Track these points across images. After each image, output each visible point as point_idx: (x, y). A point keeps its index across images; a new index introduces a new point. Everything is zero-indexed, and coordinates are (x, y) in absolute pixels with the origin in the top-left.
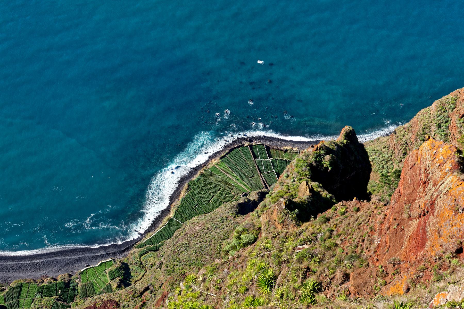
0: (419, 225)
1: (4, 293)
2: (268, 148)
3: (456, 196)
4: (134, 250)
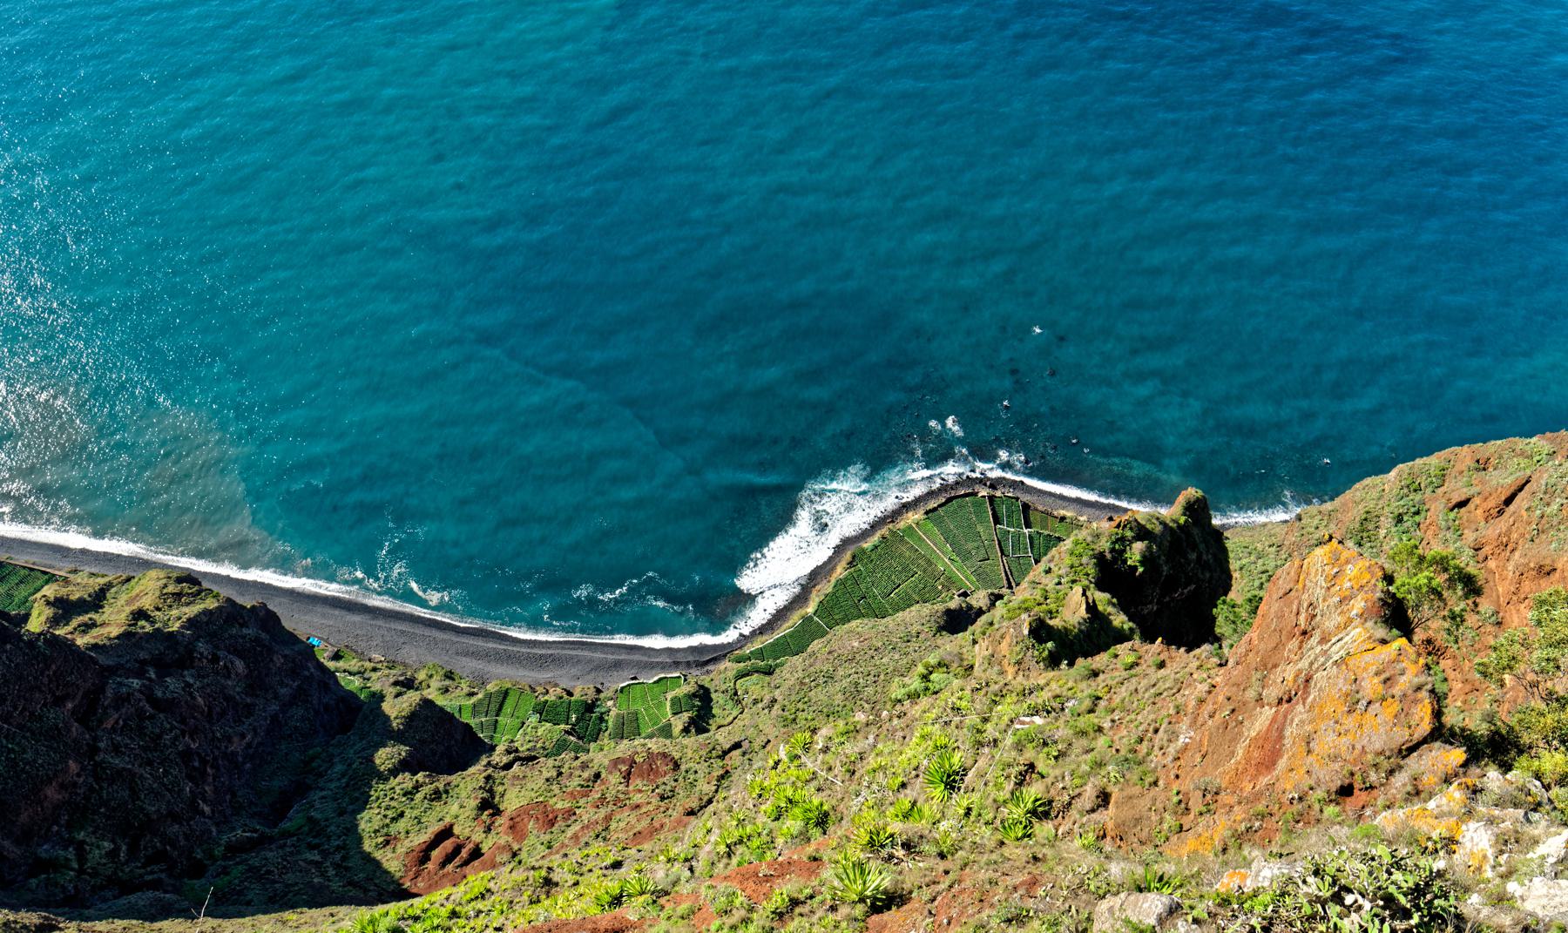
0: (1274, 720)
1: (474, 699)
2: (1026, 507)
3: (1359, 672)
4: (725, 664)
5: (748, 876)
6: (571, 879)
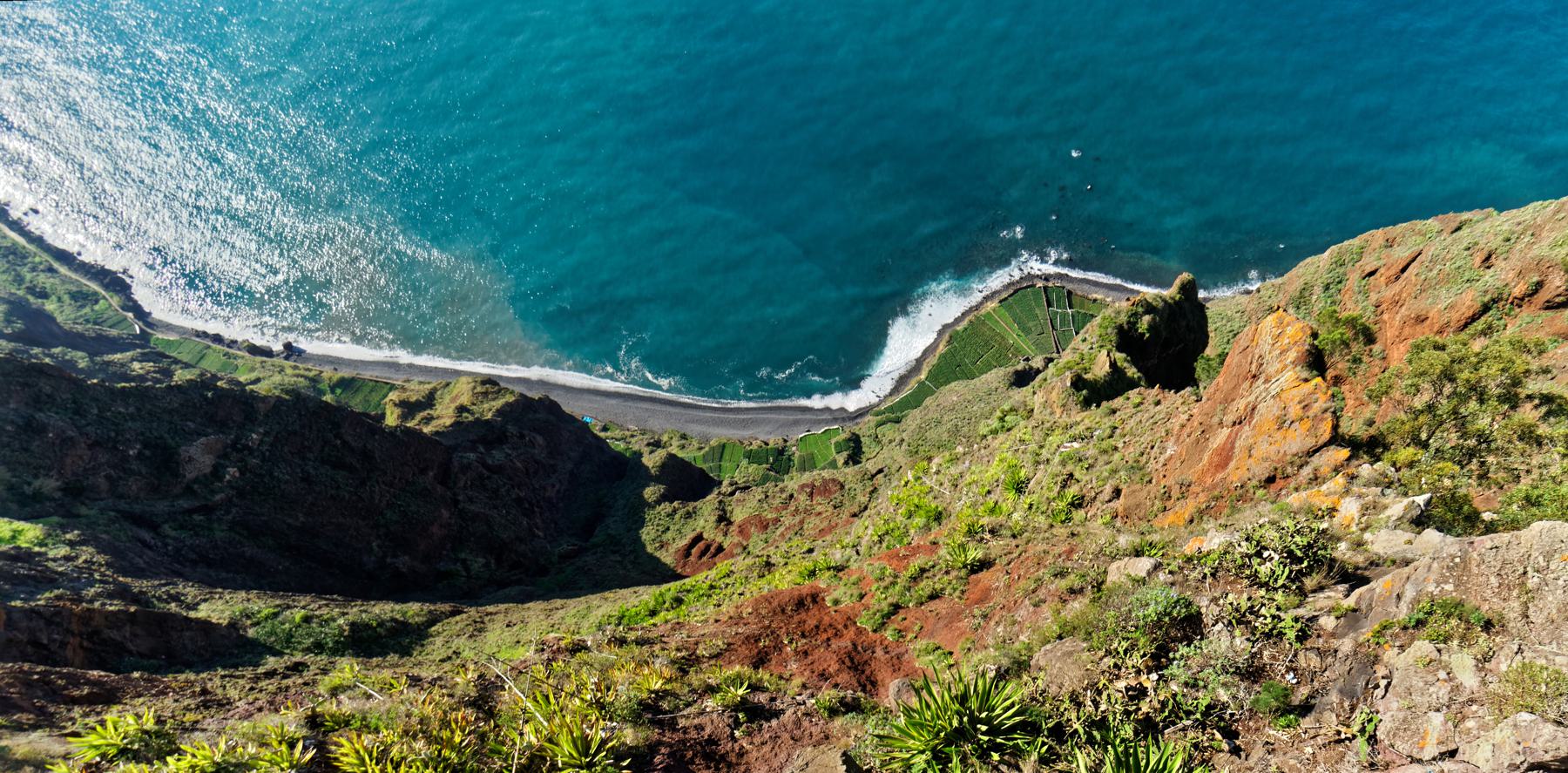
2: (1070, 293)
5: (893, 556)
6: (782, 561)
